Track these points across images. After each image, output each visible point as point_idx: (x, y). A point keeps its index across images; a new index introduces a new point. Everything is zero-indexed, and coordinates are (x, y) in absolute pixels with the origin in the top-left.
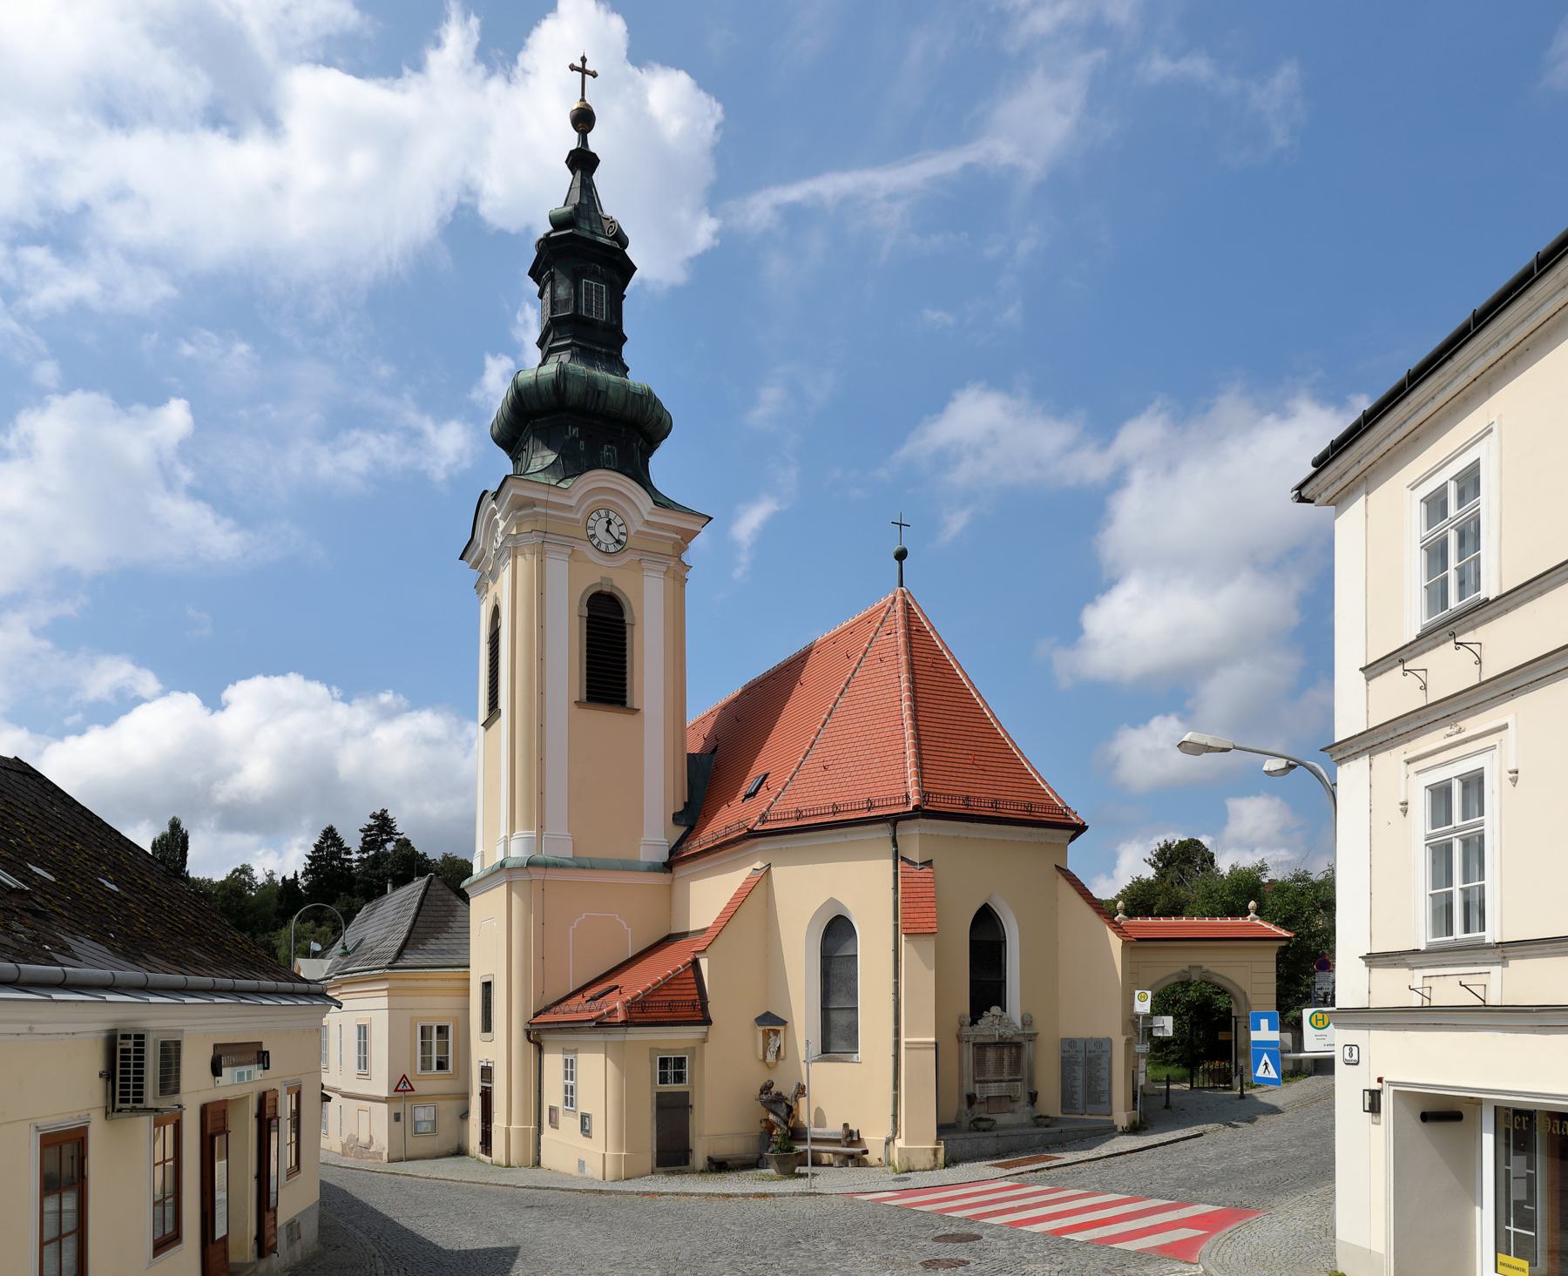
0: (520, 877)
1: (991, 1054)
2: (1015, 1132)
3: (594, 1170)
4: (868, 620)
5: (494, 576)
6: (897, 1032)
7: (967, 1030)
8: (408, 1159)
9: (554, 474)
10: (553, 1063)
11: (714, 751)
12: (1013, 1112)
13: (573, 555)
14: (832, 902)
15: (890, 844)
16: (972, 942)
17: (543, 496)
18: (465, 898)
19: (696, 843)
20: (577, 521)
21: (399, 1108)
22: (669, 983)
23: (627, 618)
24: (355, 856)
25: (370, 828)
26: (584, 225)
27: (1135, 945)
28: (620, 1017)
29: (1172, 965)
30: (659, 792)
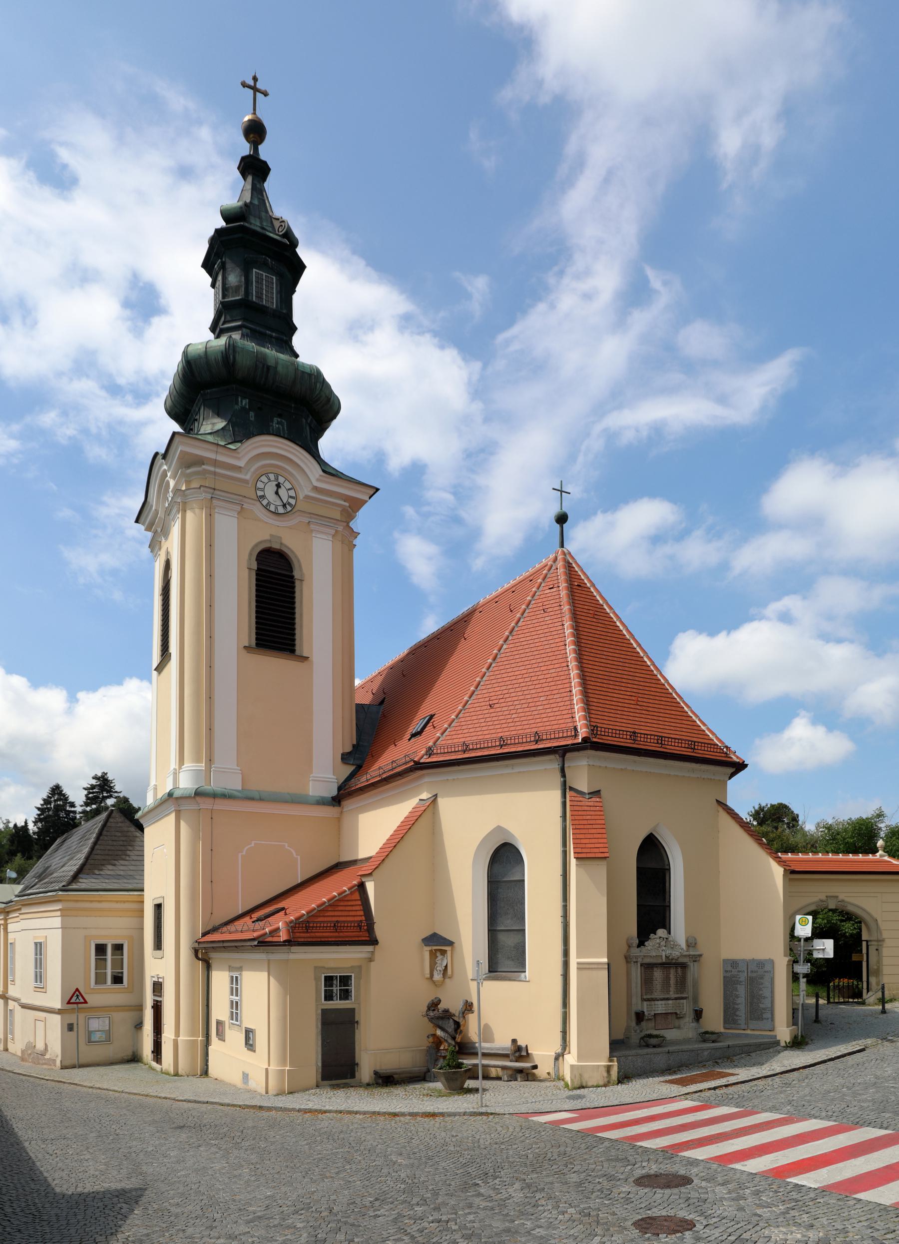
0: (187, 806)
1: (658, 974)
2: (685, 1047)
3: (257, 1083)
4: (530, 579)
5: (166, 532)
6: (566, 953)
7: (635, 952)
8: (81, 1066)
9: (224, 437)
10: (220, 979)
11: (382, 702)
12: (679, 1028)
13: (242, 511)
15: (559, 774)
16: (639, 870)
17: (212, 456)
18: (141, 828)
19: (364, 779)
20: (246, 482)
21: (72, 1018)
22: (334, 904)
23: (296, 574)
24: (79, 809)
25: (93, 787)
27: (791, 873)
28: (283, 936)
29: (819, 892)
30: (326, 739)
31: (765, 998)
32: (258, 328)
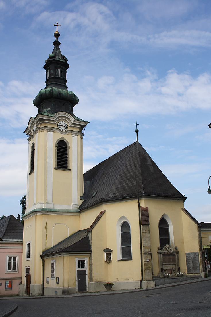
14: (123, 217)
26: (57, 57)
31: (197, 263)
32: (57, 83)
